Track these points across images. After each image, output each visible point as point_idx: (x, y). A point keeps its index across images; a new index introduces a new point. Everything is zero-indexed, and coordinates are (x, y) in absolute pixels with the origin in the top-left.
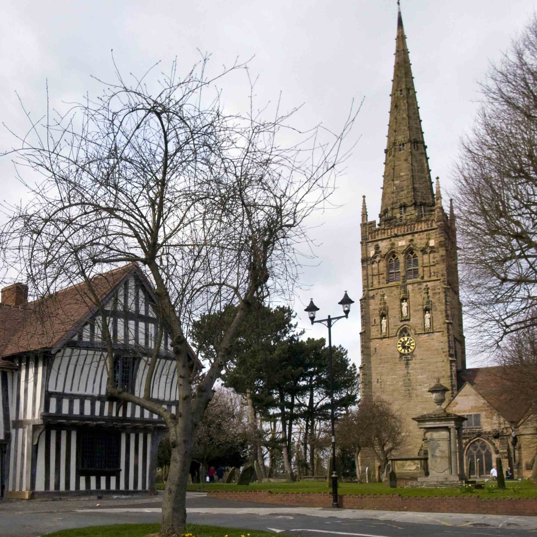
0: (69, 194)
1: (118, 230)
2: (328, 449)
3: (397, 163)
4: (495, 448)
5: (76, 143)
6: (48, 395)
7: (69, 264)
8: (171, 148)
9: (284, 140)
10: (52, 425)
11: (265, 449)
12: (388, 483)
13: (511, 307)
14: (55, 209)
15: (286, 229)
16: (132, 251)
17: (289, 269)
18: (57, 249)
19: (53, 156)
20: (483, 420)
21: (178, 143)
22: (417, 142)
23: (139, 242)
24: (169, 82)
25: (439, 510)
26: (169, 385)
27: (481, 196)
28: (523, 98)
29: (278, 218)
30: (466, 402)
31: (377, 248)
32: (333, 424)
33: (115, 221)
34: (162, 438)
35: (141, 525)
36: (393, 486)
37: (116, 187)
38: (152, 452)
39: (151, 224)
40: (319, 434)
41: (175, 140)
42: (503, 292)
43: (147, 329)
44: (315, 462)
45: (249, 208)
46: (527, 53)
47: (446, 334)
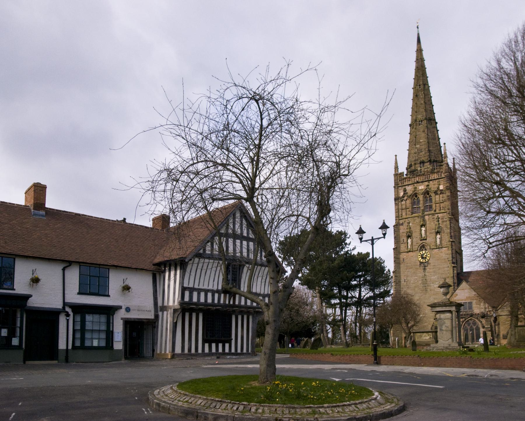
0: (197, 154)
1: (229, 178)
2: (371, 326)
3: (418, 133)
4: (482, 324)
5: (202, 121)
6: (183, 289)
7: (197, 202)
8: (265, 123)
9: (341, 117)
10: (186, 309)
11: (329, 326)
12: (411, 348)
13: (493, 230)
14: (188, 165)
15: (343, 177)
16: (238, 193)
17: (345, 205)
18: (189, 192)
19: (187, 129)
20: (474, 305)
21: (270, 120)
22: (431, 120)
23: (243, 187)
24: (264, 79)
25: (445, 366)
26: (263, 284)
27: (473, 156)
28: (501, 91)
29: (337, 170)
30: (463, 294)
31: (405, 190)
32: (374, 309)
33: (227, 173)
34: (259, 318)
35: (246, 376)
36: (414, 350)
37: (228, 149)
38: (252, 328)
39: (250, 174)
40: (365, 316)
41: (268, 118)
42: (488, 220)
43: (248, 246)
44: (362, 335)
45: (318, 163)
46: (503, 60)
47: (450, 249)
